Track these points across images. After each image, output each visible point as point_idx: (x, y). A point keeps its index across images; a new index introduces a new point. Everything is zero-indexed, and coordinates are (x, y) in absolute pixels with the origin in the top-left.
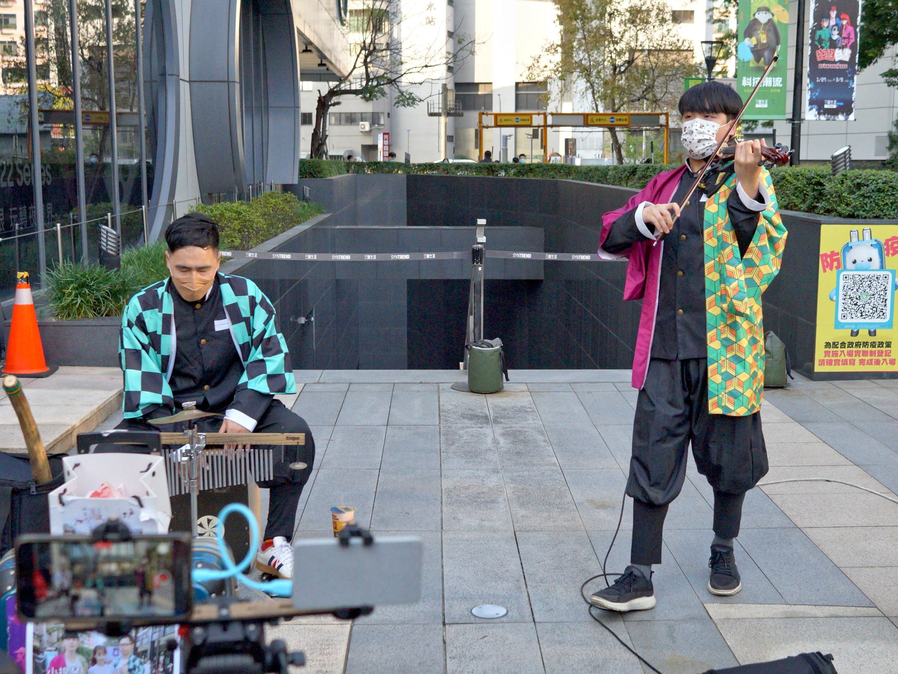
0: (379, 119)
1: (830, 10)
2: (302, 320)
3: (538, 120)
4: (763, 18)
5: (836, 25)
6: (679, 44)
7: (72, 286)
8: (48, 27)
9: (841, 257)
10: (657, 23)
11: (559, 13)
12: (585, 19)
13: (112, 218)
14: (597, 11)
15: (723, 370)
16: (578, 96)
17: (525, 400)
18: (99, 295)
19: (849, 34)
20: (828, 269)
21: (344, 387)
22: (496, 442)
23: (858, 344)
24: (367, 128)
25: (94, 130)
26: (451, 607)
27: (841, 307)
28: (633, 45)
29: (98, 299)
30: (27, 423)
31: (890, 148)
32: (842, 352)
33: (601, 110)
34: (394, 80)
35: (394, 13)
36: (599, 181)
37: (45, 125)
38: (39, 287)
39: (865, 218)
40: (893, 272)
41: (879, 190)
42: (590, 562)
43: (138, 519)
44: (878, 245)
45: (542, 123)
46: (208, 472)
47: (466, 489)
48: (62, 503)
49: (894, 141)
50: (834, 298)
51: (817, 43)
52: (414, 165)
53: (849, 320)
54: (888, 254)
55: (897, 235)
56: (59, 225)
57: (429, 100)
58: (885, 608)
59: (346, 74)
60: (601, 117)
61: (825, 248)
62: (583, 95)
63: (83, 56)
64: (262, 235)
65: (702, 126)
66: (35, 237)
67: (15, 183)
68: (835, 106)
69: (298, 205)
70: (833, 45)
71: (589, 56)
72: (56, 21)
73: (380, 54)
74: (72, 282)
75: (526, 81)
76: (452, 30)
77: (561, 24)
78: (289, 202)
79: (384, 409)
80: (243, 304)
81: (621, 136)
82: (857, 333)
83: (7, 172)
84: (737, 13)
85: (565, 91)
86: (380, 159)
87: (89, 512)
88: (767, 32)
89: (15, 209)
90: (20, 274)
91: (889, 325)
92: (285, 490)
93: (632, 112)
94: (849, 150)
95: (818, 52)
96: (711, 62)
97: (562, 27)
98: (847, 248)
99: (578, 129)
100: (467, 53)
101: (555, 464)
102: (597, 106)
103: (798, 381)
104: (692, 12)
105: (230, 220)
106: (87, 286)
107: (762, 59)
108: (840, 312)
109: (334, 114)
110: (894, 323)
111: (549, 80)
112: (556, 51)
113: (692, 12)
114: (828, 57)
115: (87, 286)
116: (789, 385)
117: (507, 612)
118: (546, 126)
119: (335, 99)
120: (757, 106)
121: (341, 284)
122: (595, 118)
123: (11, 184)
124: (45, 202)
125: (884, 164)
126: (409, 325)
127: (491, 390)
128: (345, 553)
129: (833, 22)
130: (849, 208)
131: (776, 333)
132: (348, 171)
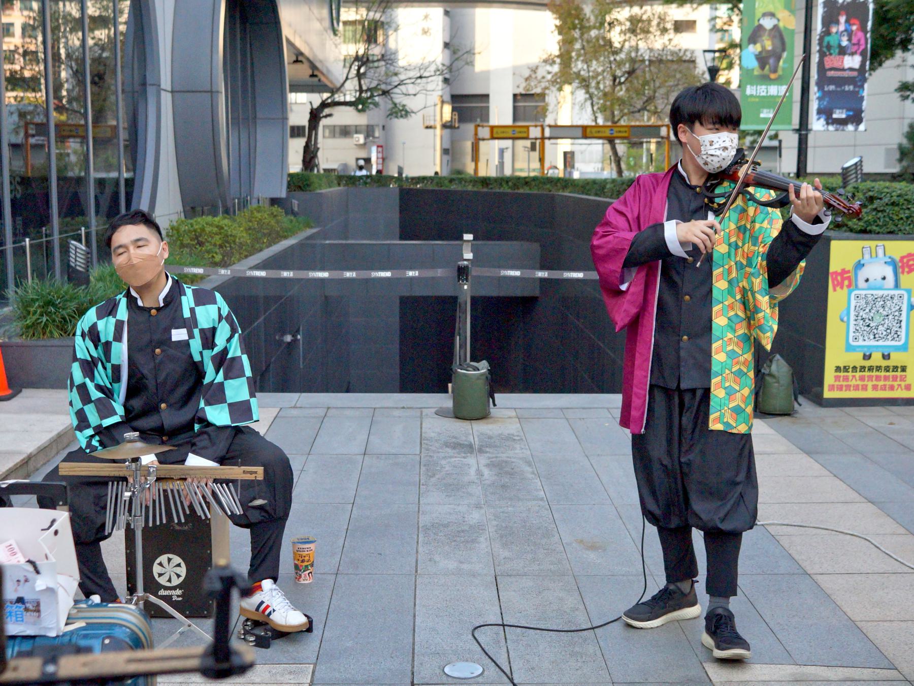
0: (373, 131)
1: (839, 14)
2: (288, 338)
3: (535, 132)
4: (768, 23)
5: (846, 30)
6: (681, 54)
7: (37, 304)
8: (36, 39)
9: (852, 275)
10: (658, 33)
11: (558, 22)
12: (584, 29)
15: (727, 384)
17: (512, 428)
18: (64, 313)
19: (859, 41)
20: (838, 289)
21: (321, 412)
22: (479, 473)
23: (871, 369)
26: (421, 664)
27: (852, 329)
28: (633, 55)
29: (64, 319)
31: (900, 160)
32: (854, 376)
33: (600, 121)
36: (596, 195)
37: (37, 138)
39: (878, 233)
40: (909, 291)
41: (893, 204)
42: (577, 613)
43: (34, 588)
44: (893, 263)
45: (539, 135)
47: (446, 526)
49: (903, 153)
50: (845, 319)
51: (825, 49)
52: (407, 178)
53: (861, 343)
54: (903, 272)
55: (913, 252)
56: (27, 240)
58: (906, 670)
59: (338, 85)
61: (835, 266)
64: (246, 250)
68: (844, 116)
69: (286, 220)
70: (843, 51)
71: (588, 66)
73: (371, 65)
75: (523, 92)
76: (447, 41)
77: (560, 33)
78: (275, 216)
81: (621, 148)
82: (870, 357)
84: (741, 21)
88: (773, 38)
91: (905, 348)
93: (633, 124)
94: (861, 161)
95: (826, 59)
96: (714, 72)
98: (859, 265)
101: (542, 499)
102: (596, 118)
103: (806, 408)
104: (694, 22)
105: (211, 235)
106: (54, 305)
107: (767, 67)
108: (851, 334)
110: (910, 346)
111: (547, 91)
113: (694, 22)
114: (836, 64)
115: (54, 305)
116: (796, 412)
117: (484, 670)
118: (543, 138)
119: (327, 111)
120: (762, 116)
121: (330, 301)
122: (594, 130)
125: (894, 177)
126: (402, 342)
127: (478, 416)
129: (842, 27)
130: (861, 223)
131: (782, 356)
132: (339, 185)
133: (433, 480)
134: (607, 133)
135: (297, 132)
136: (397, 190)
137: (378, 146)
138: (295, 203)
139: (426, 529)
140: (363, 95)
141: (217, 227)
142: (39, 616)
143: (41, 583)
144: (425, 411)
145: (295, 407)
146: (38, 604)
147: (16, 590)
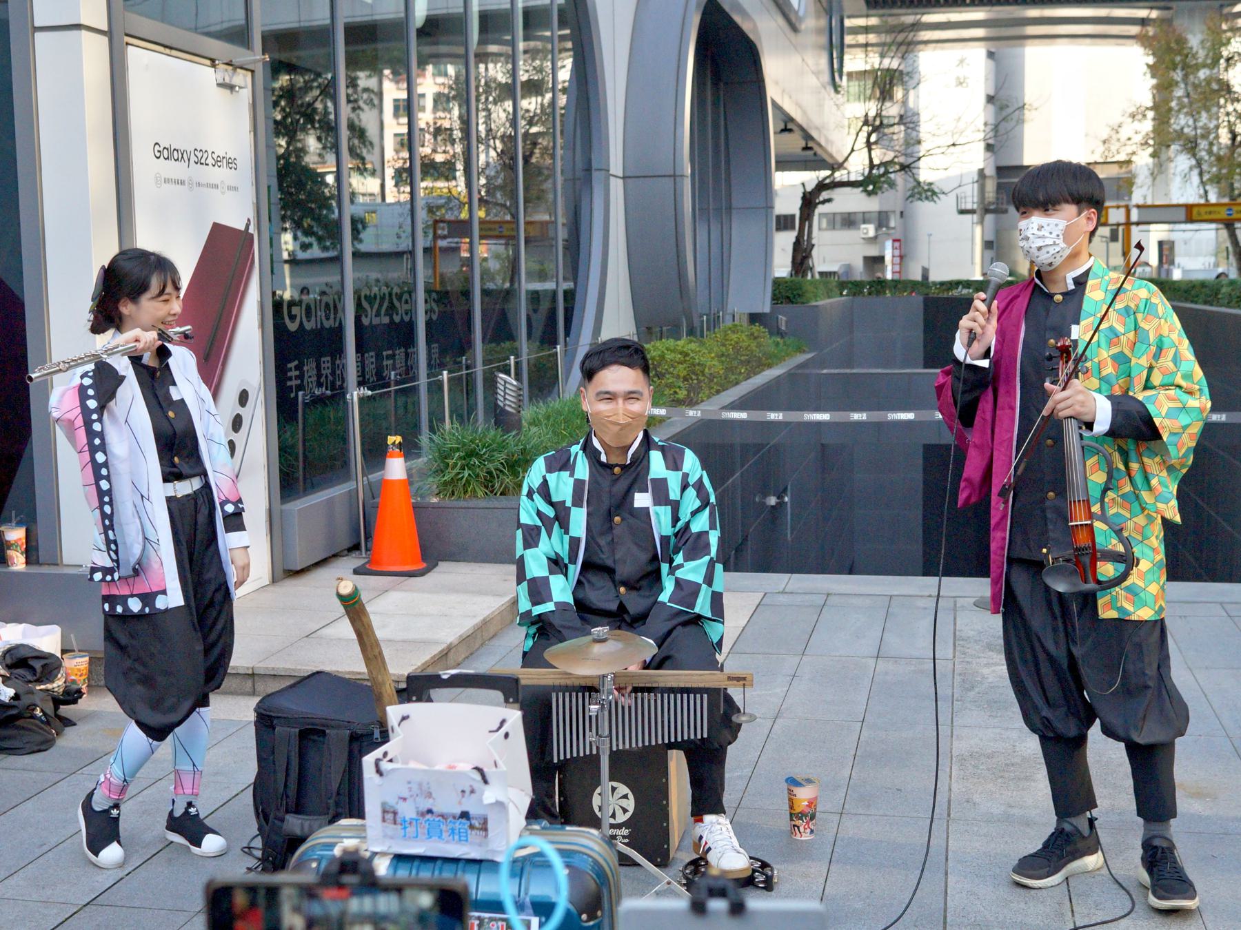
0: (888, 219)
2: (772, 501)
11: (1151, 60)
12: (1189, 68)
13: (517, 363)
16: (1178, 179)
18: (491, 466)
21: (819, 600)
24: (872, 233)
29: (490, 473)
33: (1213, 198)
34: (908, 166)
35: (908, 73)
36: (1205, 303)
38: (419, 456)
43: (481, 800)
45: (1122, 219)
46: (630, 708)
48: (379, 772)
52: (935, 283)
56: (445, 373)
60: (1212, 209)
62: (1186, 178)
63: (495, 149)
65: (1040, 228)
66: (415, 390)
69: (768, 342)
71: (1195, 121)
72: (460, 106)
73: (886, 131)
74: (458, 449)
76: (992, 93)
77: (1153, 76)
80: (674, 481)
83: (381, 306)
86: (889, 276)
87: (415, 788)
89: (390, 352)
90: (391, 439)
92: (706, 761)
102: (1206, 192)
106: (478, 455)
109: (825, 215)
112: (1144, 116)
118: (1128, 224)
119: (825, 195)
121: (828, 451)
122: (1203, 210)
123: (386, 320)
124: (428, 342)
133: (972, 694)
134: (1223, 213)
135: (784, 223)
138: (783, 319)
139: (962, 759)
140: (874, 171)
142: (486, 836)
143: (490, 795)
144: (960, 602)
145: (783, 592)
146: (485, 821)
147: (460, 803)
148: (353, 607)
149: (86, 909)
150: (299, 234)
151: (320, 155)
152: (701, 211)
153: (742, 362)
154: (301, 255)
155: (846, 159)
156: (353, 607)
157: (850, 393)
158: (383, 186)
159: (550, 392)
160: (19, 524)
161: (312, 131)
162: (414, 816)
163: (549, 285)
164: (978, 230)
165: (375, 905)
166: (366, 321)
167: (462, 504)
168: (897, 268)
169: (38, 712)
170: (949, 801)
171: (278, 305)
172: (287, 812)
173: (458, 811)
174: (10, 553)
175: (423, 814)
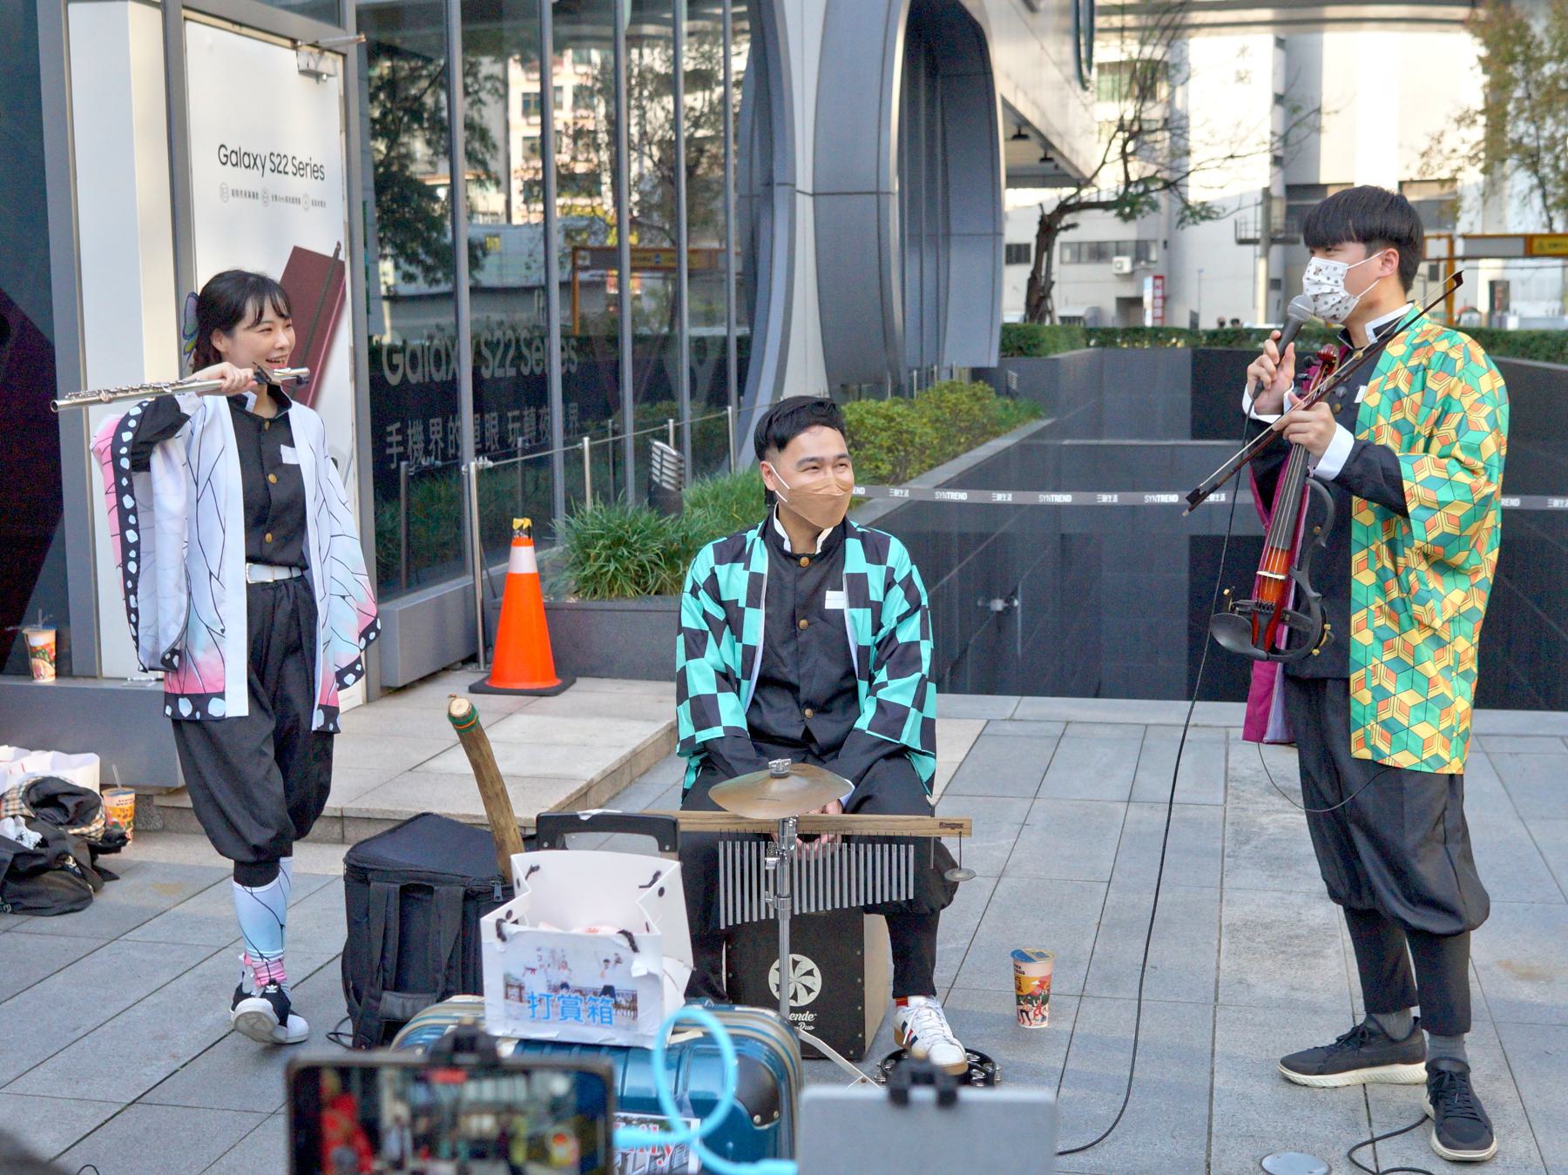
0: (1147, 251)
2: (998, 605)
7: (601, 543)
11: (1483, 52)
14: (1553, 48)
18: (643, 558)
21: (1056, 729)
24: (1127, 268)
25: (665, 279)
26: (1224, 1151)
29: (642, 566)
30: (488, 780)
36: (1548, 359)
37: (592, 272)
38: (552, 544)
42: (1497, 1084)
43: (629, 973)
45: (1444, 253)
46: (767, 888)
47: (1267, 926)
48: (501, 935)
56: (586, 439)
57: (1237, 215)
60: (1560, 241)
62: (1525, 200)
63: (651, 157)
64: (930, 456)
67: (519, 372)
71: (1538, 129)
72: (607, 103)
73: (1147, 138)
74: (602, 536)
77: (1485, 71)
78: (979, 399)
79: (1125, 774)
85: (1492, 189)
86: (1148, 322)
87: (546, 955)
89: (517, 413)
92: (913, 927)
97: (1486, 79)
99: (1513, 263)
100: (1304, 131)
102: (1551, 220)
105: (874, 431)
106: (627, 544)
112: (1474, 122)
119: (1068, 219)
121: (1068, 542)
122: (1546, 242)
123: (512, 372)
124: (565, 401)
128: (895, 1116)
135: (1017, 254)
136: (1189, 351)
137: (1156, 278)
139: (1234, 930)
140: (1131, 190)
141: (885, 417)
142: (635, 1017)
143: (640, 966)
145: (1011, 719)
147: (602, 975)
148: (469, 732)
149: (132, 1108)
150: (401, 261)
151: (431, 163)
152: (912, 237)
153: (961, 430)
154: (407, 289)
155: (1096, 173)
156: (469, 732)
157: (1096, 469)
158: (508, 203)
159: (719, 464)
160: (47, 625)
161: (418, 133)
162: (545, 991)
163: (719, 331)
164: (1262, 265)
165: (497, 1089)
166: (486, 374)
167: (607, 605)
168: (1159, 313)
169: (71, 863)
170: (1217, 982)
171: (375, 353)
172: (384, 988)
173: (600, 985)
174: (36, 662)
175: (555, 989)
